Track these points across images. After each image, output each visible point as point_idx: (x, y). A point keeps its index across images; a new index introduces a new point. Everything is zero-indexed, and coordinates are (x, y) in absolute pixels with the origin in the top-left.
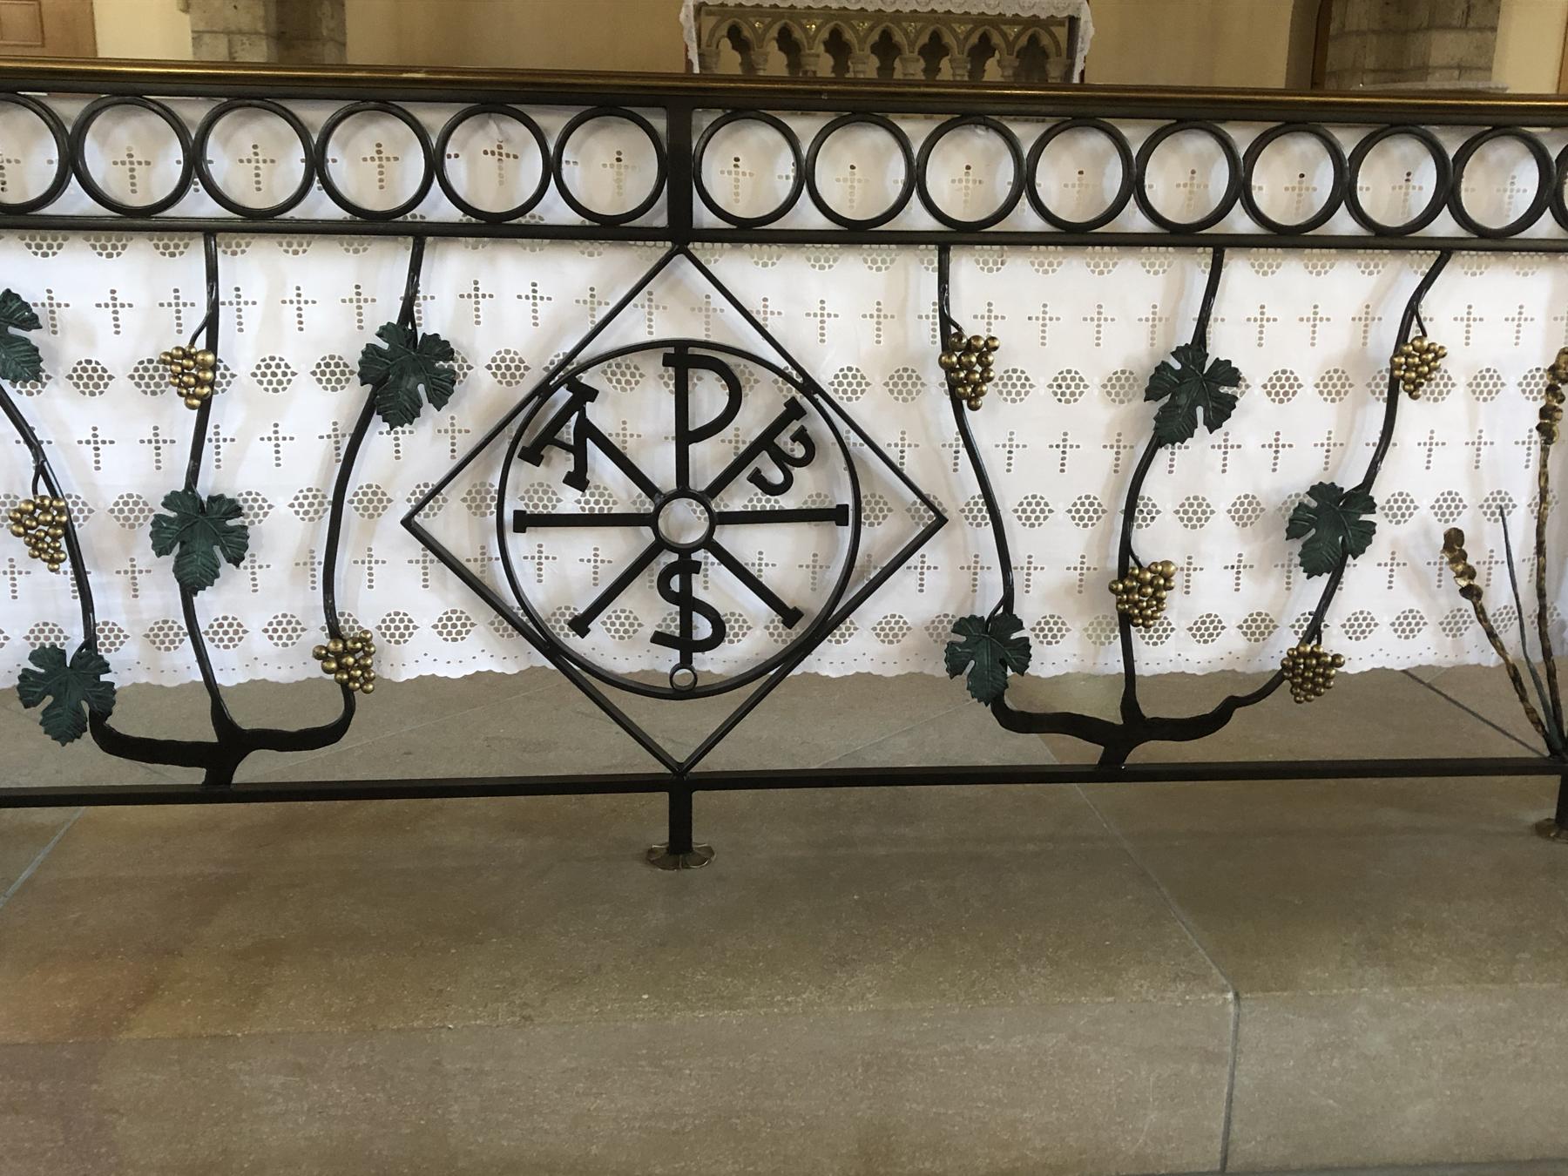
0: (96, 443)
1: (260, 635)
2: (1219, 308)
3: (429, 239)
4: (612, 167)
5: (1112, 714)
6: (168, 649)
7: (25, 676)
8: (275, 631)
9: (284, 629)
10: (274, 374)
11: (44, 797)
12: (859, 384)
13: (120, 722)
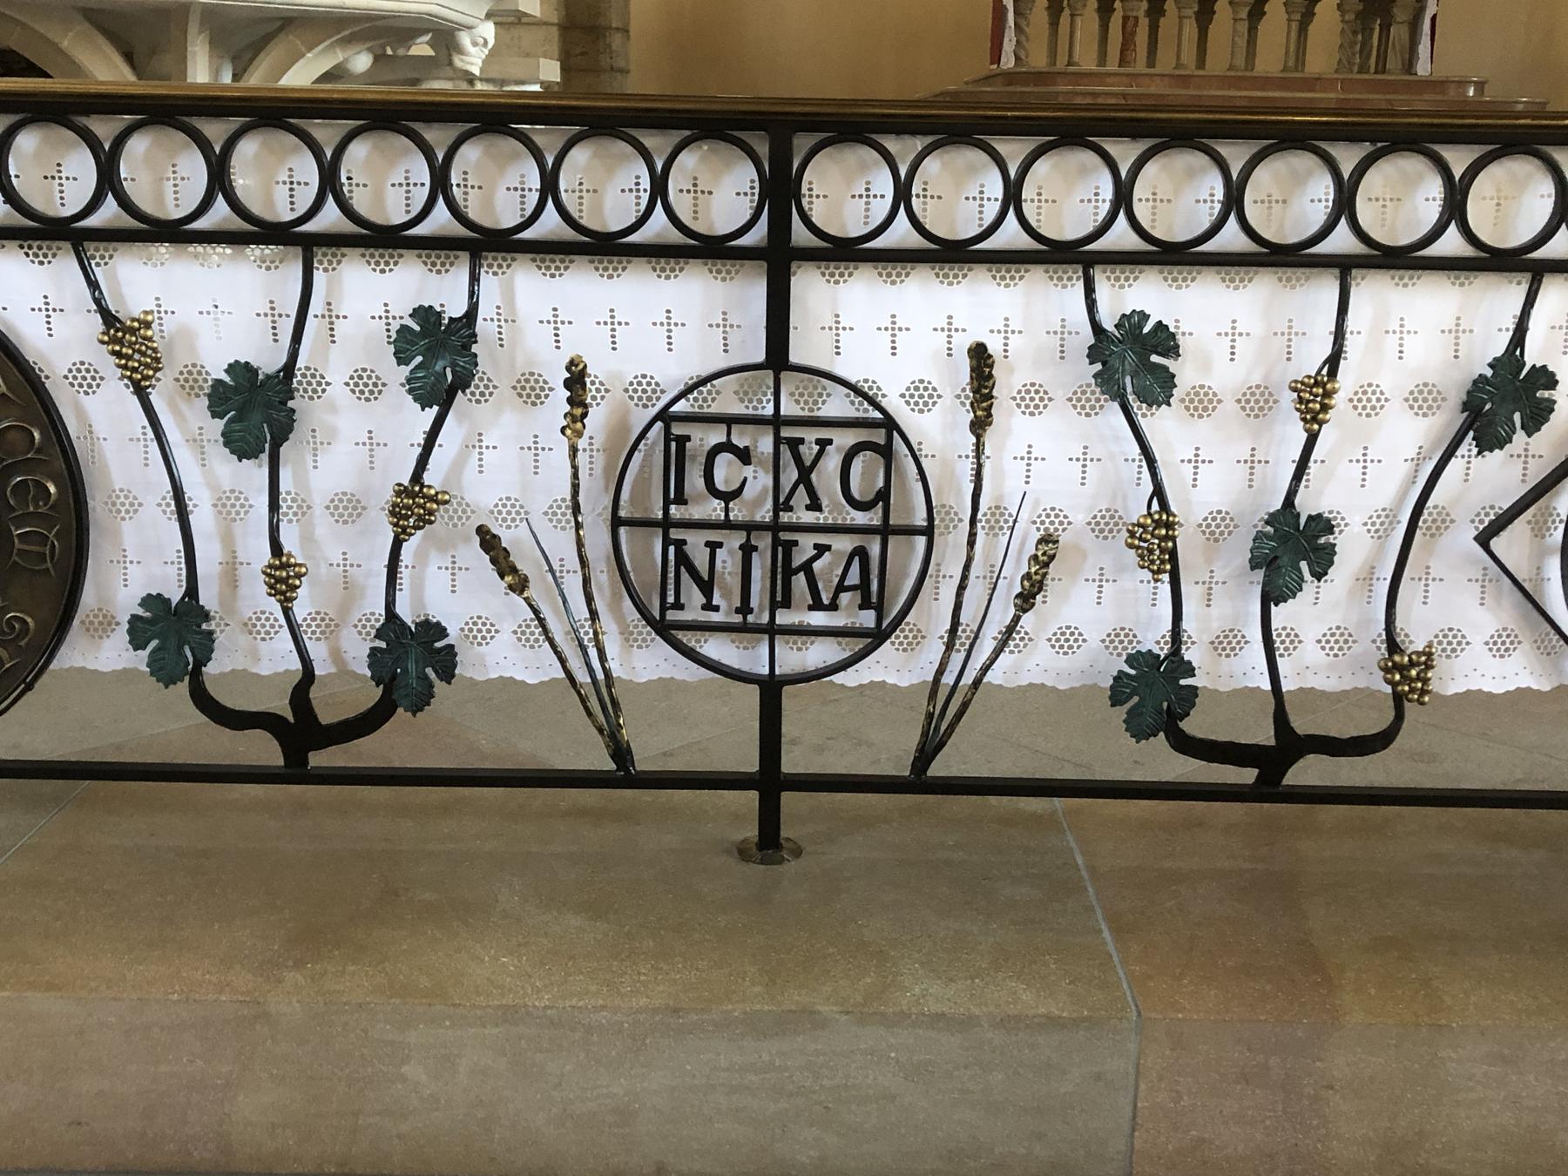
0: (1196, 461)
1: (1322, 644)
2: (1351, 323)
3: (1354, 272)
4: (723, 192)
5: (1264, 735)
6: (1228, 656)
7: (1120, 677)
8: (1328, 642)
9: (1336, 641)
10: (1370, 402)
11: (1356, 796)
12: (1042, 399)
13: (1193, 725)
